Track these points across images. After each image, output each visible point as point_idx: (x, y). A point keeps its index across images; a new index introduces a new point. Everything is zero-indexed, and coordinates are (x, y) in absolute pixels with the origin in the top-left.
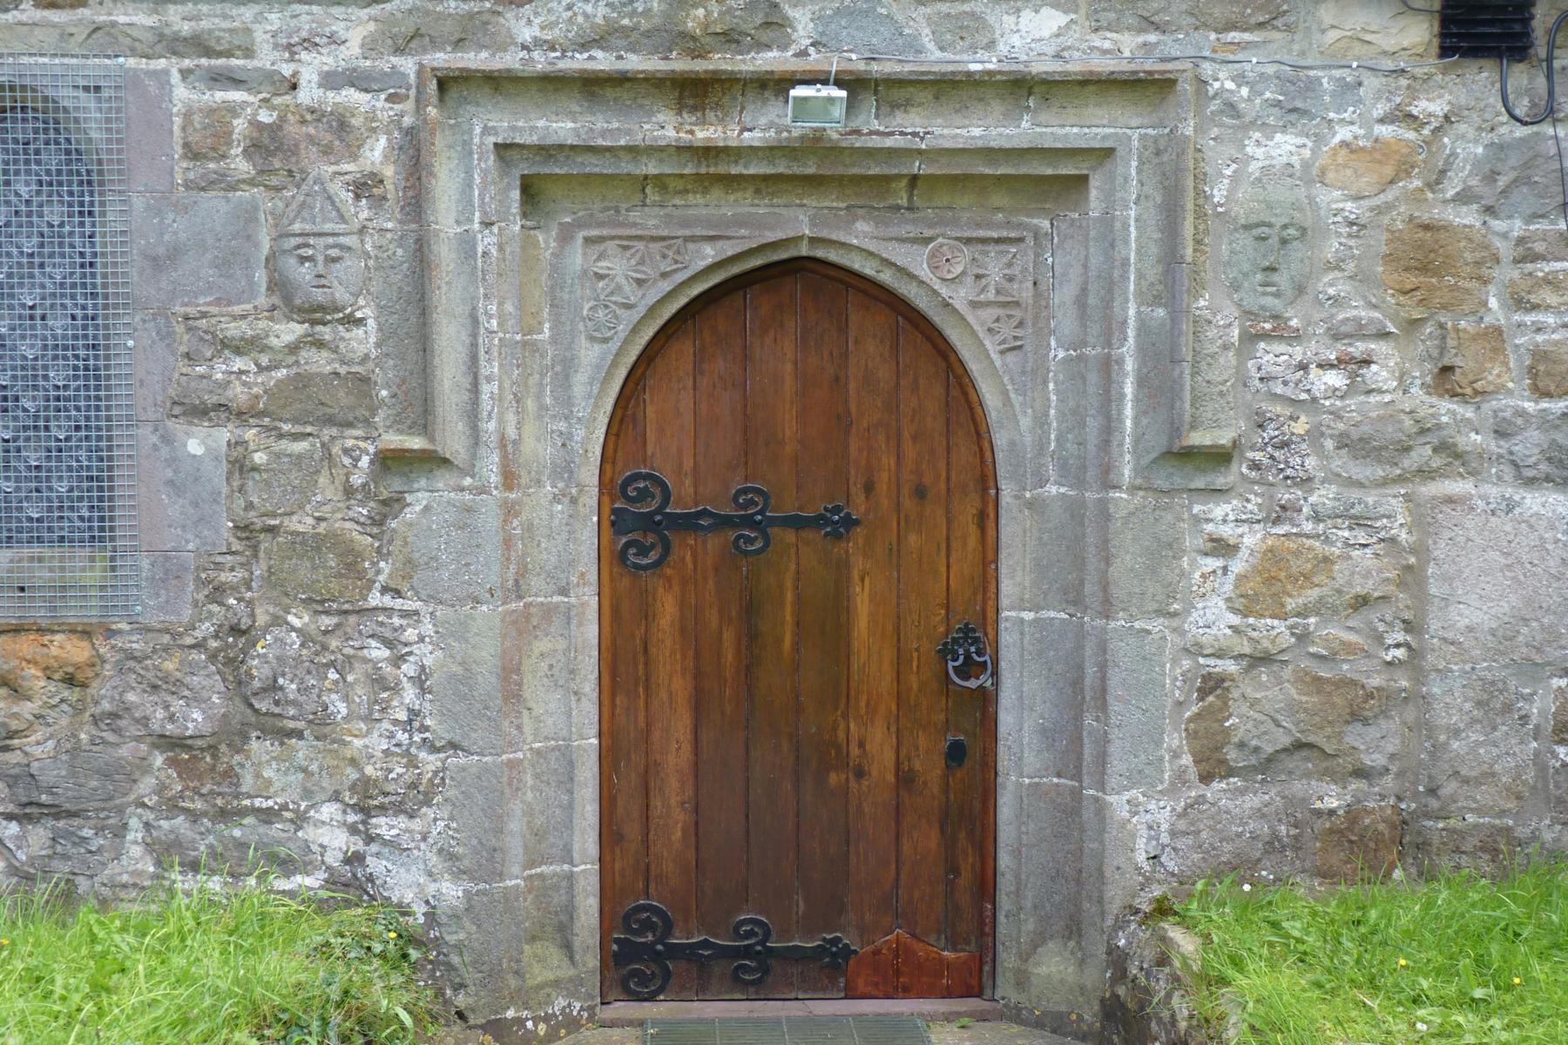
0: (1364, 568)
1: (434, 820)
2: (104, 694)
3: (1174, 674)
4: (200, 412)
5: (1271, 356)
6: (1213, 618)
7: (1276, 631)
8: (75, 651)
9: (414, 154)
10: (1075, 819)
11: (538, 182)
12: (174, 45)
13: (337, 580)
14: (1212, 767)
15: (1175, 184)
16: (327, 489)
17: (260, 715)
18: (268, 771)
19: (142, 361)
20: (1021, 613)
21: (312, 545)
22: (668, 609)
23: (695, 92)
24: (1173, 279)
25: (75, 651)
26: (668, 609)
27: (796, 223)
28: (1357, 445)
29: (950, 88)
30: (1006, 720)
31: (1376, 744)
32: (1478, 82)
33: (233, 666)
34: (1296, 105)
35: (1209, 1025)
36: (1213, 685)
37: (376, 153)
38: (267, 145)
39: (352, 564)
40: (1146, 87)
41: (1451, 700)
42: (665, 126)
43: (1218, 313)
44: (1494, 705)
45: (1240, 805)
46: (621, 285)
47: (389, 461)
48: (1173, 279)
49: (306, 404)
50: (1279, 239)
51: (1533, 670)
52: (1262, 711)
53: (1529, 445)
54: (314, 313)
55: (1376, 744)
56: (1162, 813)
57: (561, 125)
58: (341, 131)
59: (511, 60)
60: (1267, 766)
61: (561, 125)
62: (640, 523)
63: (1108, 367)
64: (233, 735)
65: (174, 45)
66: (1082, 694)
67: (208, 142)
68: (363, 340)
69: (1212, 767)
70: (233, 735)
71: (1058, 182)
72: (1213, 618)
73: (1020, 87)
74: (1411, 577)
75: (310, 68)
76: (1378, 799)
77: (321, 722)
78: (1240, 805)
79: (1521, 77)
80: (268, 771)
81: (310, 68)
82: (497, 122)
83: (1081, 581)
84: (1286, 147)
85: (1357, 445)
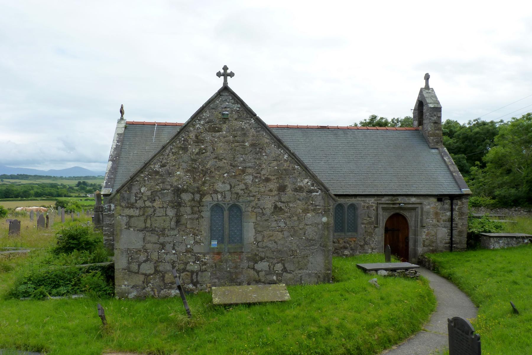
0: (433, 233)
1: (377, 250)
2: (356, 242)
3: (422, 240)
4: (363, 224)
5: (428, 220)
6: (424, 237)
7: (428, 237)
8: (354, 239)
9: (377, 208)
10: (415, 251)
11: (383, 209)
12: (362, 201)
13: (371, 234)
14: (424, 246)
15: (422, 209)
16: (370, 229)
17: (366, 243)
18: (366, 247)
19: (359, 221)
20: (411, 236)
21: (370, 232)
22: (388, 236)
23: (394, 204)
24: (422, 215)
25: (354, 239)
26: (388, 236)
27: (398, 211)
28: (433, 225)
29: (409, 204)
30: (410, 243)
31: (434, 245)
32: (440, 203)
33: (364, 240)
34: (429, 204)
35: (530, 182)
36: (424, 241)
37: (374, 207)
38: (367, 207)
39: (372, 233)
40: (421, 204)
41: (438, 242)
42: (392, 206)
43: (424, 217)
44: (441, 242)
45: (426, 249)
46: (387, 215)
47: (375, 227)
48: (422, 215)
49: (370, 223)
50: (428, 213)
51: (443, 240)
52: (427, 242)
53: (443, 225)
54: (370, 218)
55: (434, 245)
56: (421, 249)
57: (385, 206)
58: (372, 206)
59: (382, 202)
60: (427, 246)
61: (385, 206)
62: (387, 230)
63: (418, 221)
64: (364, 245)
65: (362, 201)
66: (415, 242)
67: (364, 207)
68: (373, 219)
69: (424, 246)
70: (364, 245)
71: (414, 209)
72: (424, 237)
73: (413, 204)
74: (436, 234)
75: (370, 202)
76: (434, 248)
77: (370, 244)
78: (426, 249)
79: (442, 203)
80: (366, 247)
81: (370, 202)
82: (381, 206)
83: (416, 234)
84: (428, 207)
85: (433, 225)
